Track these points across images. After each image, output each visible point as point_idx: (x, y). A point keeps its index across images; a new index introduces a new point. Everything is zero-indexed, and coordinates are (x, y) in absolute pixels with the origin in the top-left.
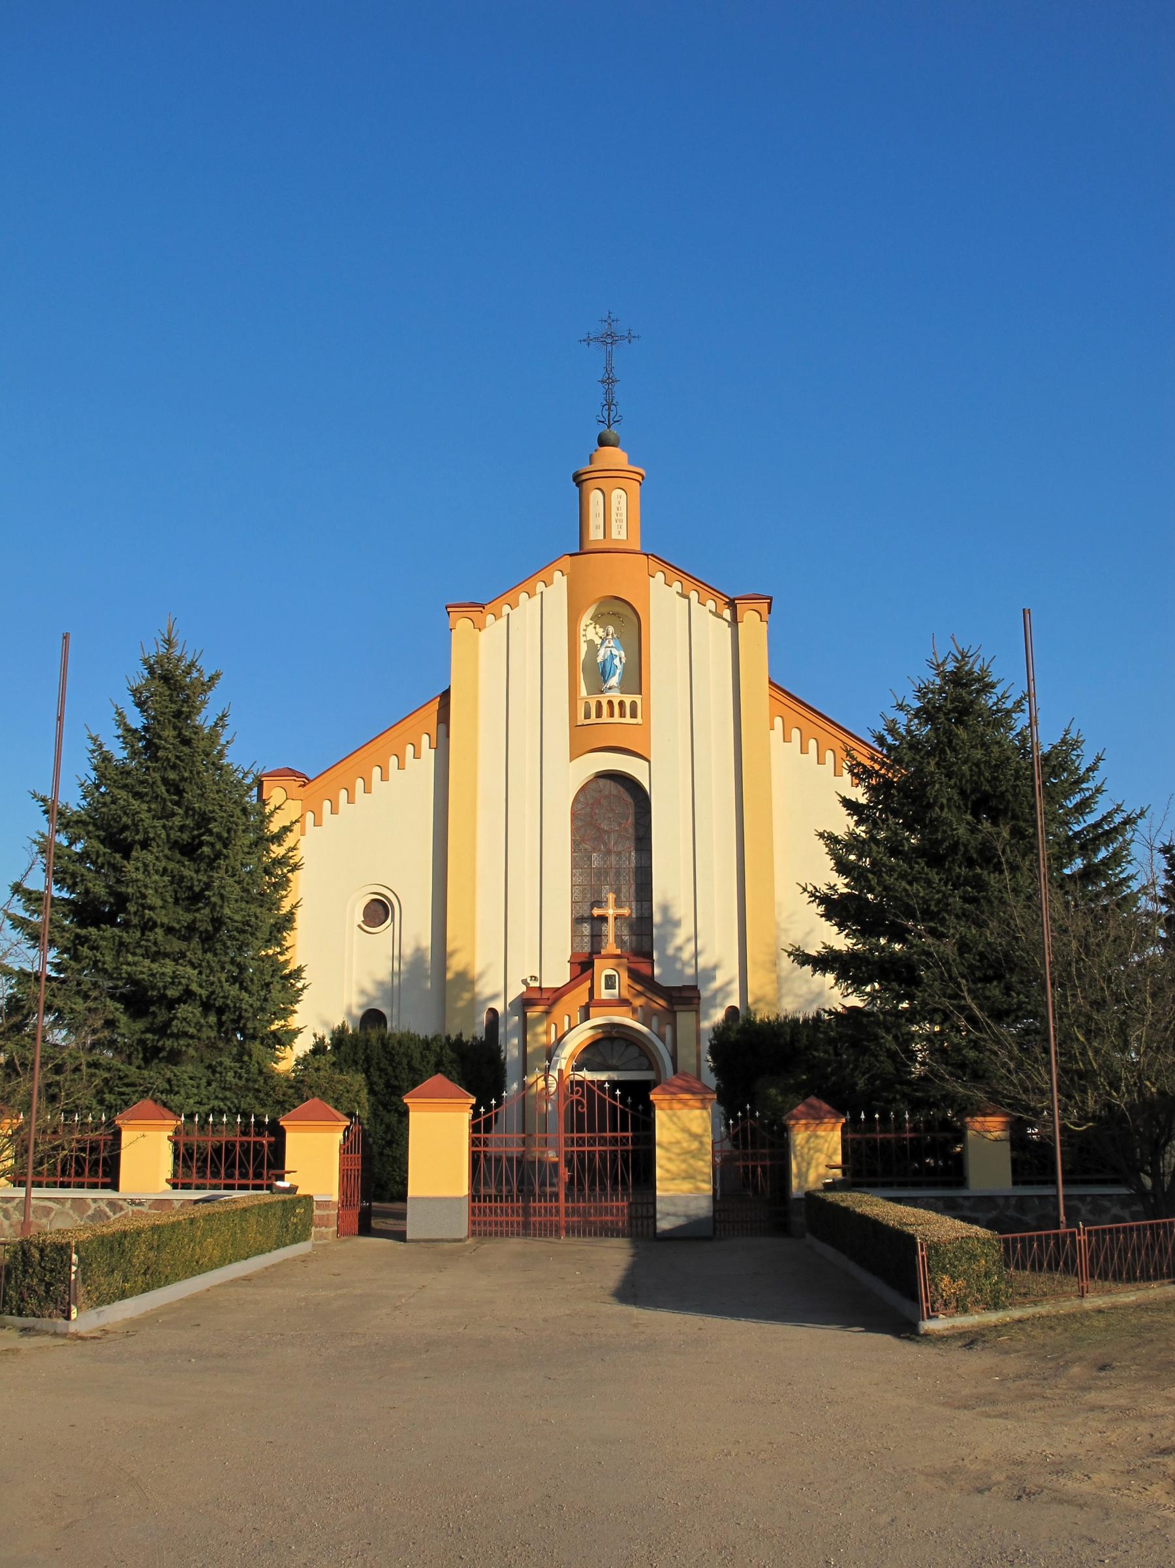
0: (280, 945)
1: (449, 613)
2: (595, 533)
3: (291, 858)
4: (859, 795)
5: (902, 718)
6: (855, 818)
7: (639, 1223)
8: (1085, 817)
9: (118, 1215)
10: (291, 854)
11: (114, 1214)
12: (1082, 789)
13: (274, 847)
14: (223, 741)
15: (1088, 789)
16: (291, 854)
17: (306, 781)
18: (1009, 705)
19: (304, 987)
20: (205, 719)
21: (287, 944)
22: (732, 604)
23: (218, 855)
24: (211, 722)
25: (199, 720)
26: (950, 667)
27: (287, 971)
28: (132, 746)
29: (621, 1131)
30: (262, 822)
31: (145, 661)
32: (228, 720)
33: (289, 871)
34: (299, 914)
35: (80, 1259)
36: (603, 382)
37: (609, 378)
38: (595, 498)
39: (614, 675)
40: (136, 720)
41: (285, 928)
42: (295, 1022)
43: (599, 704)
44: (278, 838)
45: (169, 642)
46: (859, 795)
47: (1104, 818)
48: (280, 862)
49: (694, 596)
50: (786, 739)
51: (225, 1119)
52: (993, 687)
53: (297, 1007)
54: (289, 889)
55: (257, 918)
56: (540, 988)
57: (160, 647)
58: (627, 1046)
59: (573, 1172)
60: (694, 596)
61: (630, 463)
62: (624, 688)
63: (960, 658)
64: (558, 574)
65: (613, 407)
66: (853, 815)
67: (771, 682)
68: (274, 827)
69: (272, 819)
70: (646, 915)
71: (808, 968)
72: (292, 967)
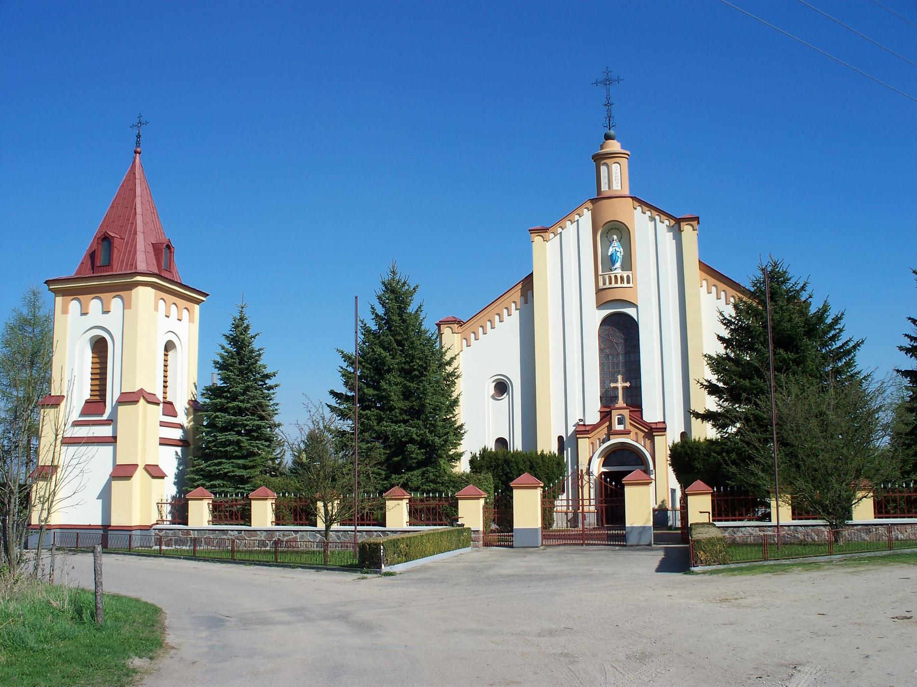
0: (452, 413)
2: (604, 187)
4: (726, 334)
6: (725, 345)
7: (619, 539)
10: (456, 371)
13: (447, 367)
14: (421, 318)
16: (456, 371)
17: (460, 323)
19: (465, 432)
20: (412, 309)
22: (678, 221)
23: (422, 374)
26: (769, 269)
30: (441, 357)
31: (383, 283)
33: (455, 378)
34: (461, 399)
35: (384, 547)
37: (608, 103)
38: (603, 169)
39: (617, 262)
40: (380, 311)
42: (460, 449)
43: (610, 278)
44: (449, 363)
45: (393, 272)
46: (726, 334)
47: (843, 345)
48: (452, 374)
49: (657, 218)
50: (709, 292)
51: (431, 495)
54: (455, 387)
55: (441, 403)
56: (584, 425)
57: (390, 276)
60: (657, 218)
61: (622, 148)
62: (623, 268)
64: (585, 210)
65: (611, 118)
66: (724, 344)
67: (699, 261)
68: (447, 358)
72: (458, 424)
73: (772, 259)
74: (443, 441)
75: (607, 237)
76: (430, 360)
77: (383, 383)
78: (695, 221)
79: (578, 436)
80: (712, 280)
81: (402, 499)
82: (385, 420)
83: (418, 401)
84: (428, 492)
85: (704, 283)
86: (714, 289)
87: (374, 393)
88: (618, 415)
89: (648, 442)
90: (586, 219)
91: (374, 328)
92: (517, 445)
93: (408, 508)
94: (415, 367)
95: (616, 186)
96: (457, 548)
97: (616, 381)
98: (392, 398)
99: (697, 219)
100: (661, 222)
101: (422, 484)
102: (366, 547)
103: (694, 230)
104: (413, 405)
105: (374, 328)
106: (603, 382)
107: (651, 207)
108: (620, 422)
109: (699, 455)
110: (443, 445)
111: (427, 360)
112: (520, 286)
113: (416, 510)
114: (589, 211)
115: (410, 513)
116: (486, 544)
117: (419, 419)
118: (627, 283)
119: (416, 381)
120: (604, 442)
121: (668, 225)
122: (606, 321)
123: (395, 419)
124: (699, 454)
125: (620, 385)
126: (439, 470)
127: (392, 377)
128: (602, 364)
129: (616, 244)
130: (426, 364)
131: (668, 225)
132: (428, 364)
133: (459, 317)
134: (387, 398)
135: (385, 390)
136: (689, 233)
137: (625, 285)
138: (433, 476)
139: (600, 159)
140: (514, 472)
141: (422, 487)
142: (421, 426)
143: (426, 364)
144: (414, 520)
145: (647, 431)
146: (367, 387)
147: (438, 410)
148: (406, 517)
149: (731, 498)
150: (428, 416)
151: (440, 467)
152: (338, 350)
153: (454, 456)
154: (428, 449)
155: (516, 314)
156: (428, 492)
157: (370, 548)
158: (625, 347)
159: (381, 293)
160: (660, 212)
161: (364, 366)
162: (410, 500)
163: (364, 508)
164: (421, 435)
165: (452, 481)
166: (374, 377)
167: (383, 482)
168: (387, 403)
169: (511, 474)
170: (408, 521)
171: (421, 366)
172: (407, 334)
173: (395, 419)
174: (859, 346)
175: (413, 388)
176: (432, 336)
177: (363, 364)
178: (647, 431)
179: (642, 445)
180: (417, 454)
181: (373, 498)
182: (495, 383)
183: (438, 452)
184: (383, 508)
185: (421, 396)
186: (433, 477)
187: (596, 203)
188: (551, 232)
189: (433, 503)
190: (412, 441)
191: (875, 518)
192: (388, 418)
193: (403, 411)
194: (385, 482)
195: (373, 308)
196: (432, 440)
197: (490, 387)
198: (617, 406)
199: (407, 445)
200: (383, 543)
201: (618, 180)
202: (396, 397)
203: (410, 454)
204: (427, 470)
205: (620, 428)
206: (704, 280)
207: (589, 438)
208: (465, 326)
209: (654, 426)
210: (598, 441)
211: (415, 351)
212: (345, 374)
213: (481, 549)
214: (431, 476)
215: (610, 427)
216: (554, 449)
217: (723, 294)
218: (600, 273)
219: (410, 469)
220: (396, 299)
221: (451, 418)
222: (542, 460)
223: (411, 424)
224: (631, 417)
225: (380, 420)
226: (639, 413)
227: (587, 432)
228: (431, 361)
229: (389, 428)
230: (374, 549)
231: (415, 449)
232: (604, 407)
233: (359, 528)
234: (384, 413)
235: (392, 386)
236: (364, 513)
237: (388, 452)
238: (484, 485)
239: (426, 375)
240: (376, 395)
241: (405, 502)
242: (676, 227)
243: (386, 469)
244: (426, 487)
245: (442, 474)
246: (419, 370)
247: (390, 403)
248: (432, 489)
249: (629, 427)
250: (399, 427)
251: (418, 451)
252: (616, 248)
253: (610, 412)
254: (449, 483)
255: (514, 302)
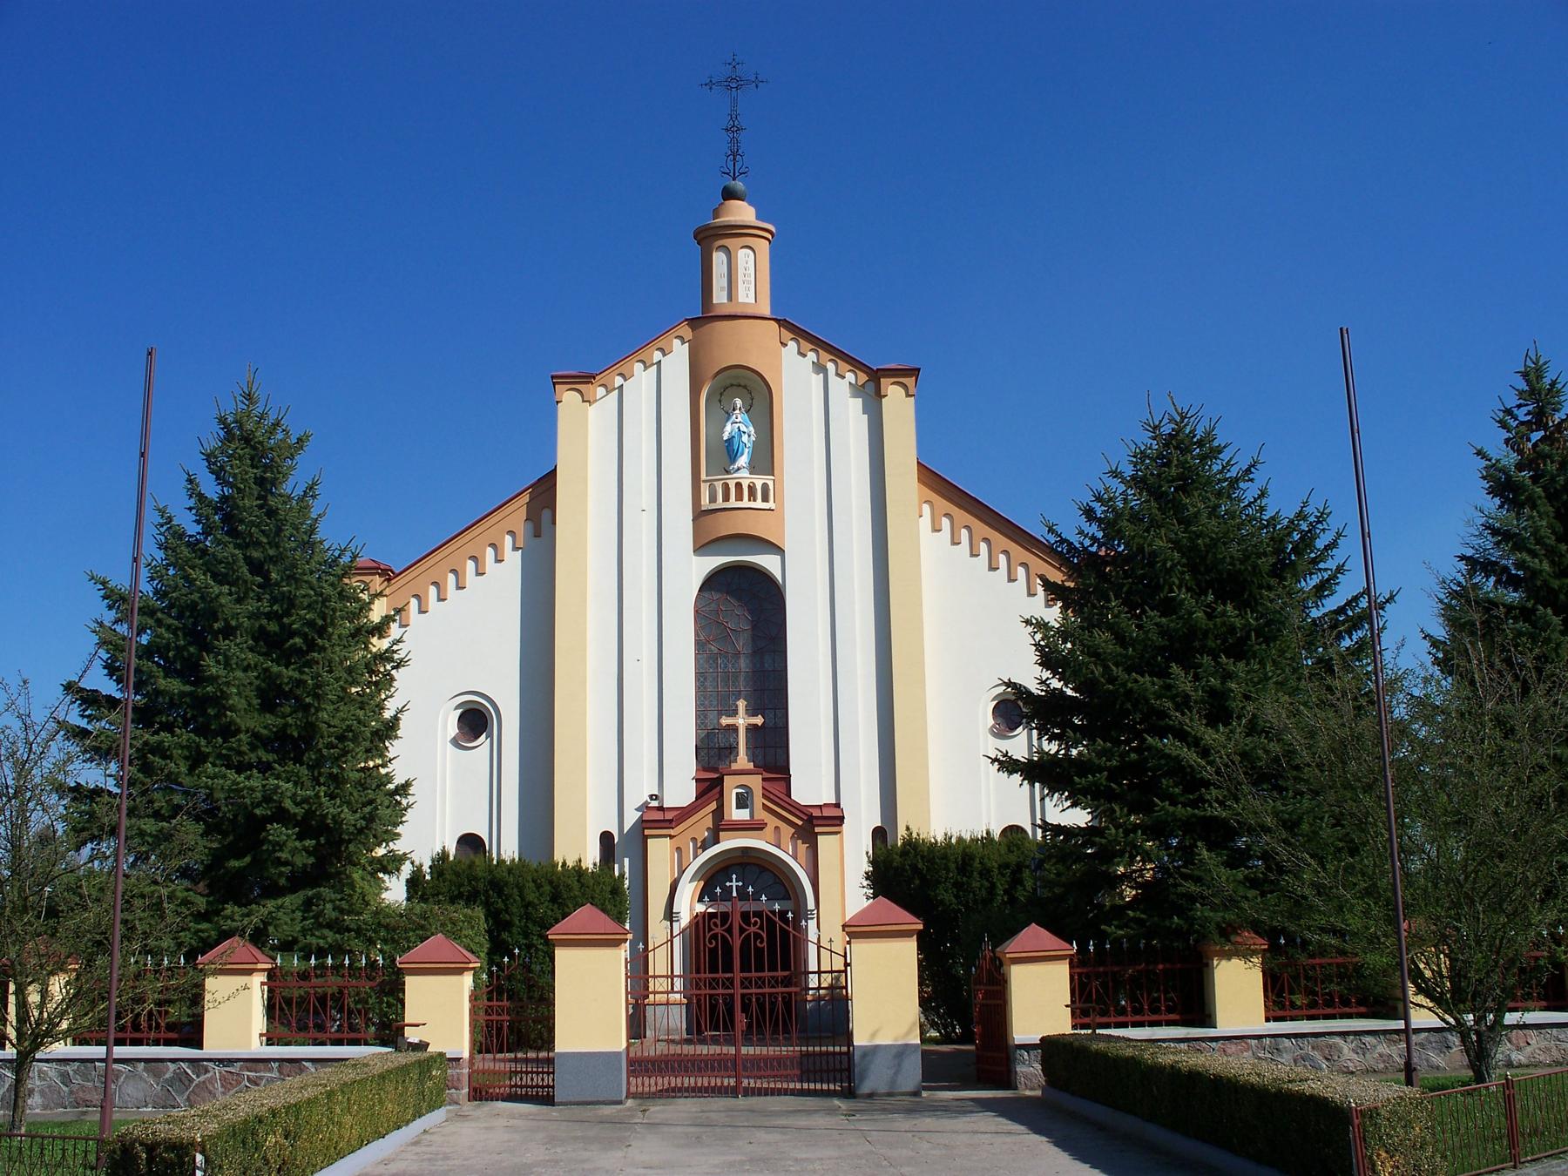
0: (382, 756)
1: (554, 384)
2: (719, 296)
3: (395, 652)
5: (1118, 487)
8: (1323, 601)
9: (202, 1078)
10: (395, 648)
11: (198, 1077)
12: (1320, 570)
13: (374, 640)
15: (1326, 570)
16: (395, 648)
18: (1233, 473)
20: (293, 485)
21: (390, 755)
23: (312, 646)
24: (299, 491)
25: (287, 488)
26: (1167, 429)
27: (391, 787)
28: (208, 519)
29: (769, 971)
31: (222, 421)
32: (318, 489)
33: (393, 668)
35: (207, 1160)
36: (727, 130)
38: (719, 259)
39: (742, 454)
40: (211, 489)
41: (389, 738)
42: (399, 846)
43: (726, 488)
44: (380, 629)
45: (249, 397)
47: (1349, 603)
48: (385, 656)
49: (831, 367)
51: (330, 961)
52: (1220, 452)
53: (399, 829)
55: (359, 722)
56: (661, 808)
58: (761, 873)
59: (751, 1018)
60: (831, 367)
61: (757, 219)
62: (754, 468)
63: (1178, 419)
64: (677, 342)
67: (918, 462)
69: (372, 606)
70: (781, 725)
71: (1017, 777)
72: (399, 780)
73: (1176, 410)
74: (363, 818)
75: (720, 401)
76: (334, 610)
77: (208, 660)
78: (911, 376)
79: (647, 832)
80: (944, 505)
81: (249, 972)
82: (210, 759)
83: (300, 715)
84: (321, 953)
85: (926, 508)
86: (946, 522)
87: (182, 688)
88: (737, 787)
89: (802, 848)
90: (677, 360)
91: (193, 529)
92: (509, 848)
93: (265, 996)
94: (294, 626)
95: (746, 296)
96: (418, 1114)
97: (735, 713)
98: (231, 702)
99: (914, 372)
100: (838, 374)
101: (304, 932)
102: (137, 1157)
103: (908, 395)
104: (286, 725)
105: (193, 529)
106: (701, 715)
107: (819, 344)
108: (742, 802)
109: (947, 873)
110: (361, 831)
111: (326, 607)
112: (526, 498)
113: (289, 1002)
114: (683, 343)
115: (270, 1009)
116: (479, 1094)
117: (298, 760)
118: (763, 501)
119: (295, 663)
120: (704, 847)
121: (854, 382)
122: (712, 583)
123: (235, 759)
124: (948, 870)
125: (742, 721)
126: (350, 895)
127: (238, 648)
128: (701, 677)
129: (740, 416)
130: (325, 620)
131: (854, 382)
132: (329, 621)
133: (385, 561)
134: (219, 701)
135: (213, 679)
136: (898, 403)
137: (759, 504)
138: (334, 910)
139: (710, 236)
140: (515, 910)
141: (303, 941)
142: (305, 779)
143: (325, 620)
144: (282, 1030)
145: (800, 823)
146: (166, 677)
147: (351, 740)
148: (258, 1022)
149: (1179, 966)
150: (322, 756)
151: (353, 887)
152: (93, 578)
153: (385, 863)
154: (322, 840)
155: (513, 560)
156: (321, 953)
157: (150, 1160)
158: (753, 640)
159: (212, 443)
160: (838, 354)
161: (159, 623)
162: (271, 974)
163: (139, 1000)
164: (306, 800)
165: (383, 926)
166: (184, 648)
167: (199, 927)
168: (217, 716)
169: (507, 912)
170: (265, 1032)
171: (311, 624)
172: (277, 546)
173: (235, 759)
174: (1383, 609)
175: (286, 680)
176: (339, 556)
177: (159, 615)
178: (800, 823)
179: (788, 855)
180: (294, 851)
181: (169, 969)
182: (459, 711)
183: (347, 848)
184: (196, 999)
185: (307, 700)
186: (334, 915)
187: (701, 326)
188: (599, 383)
189: (332, 983)
190: (281, 816)
191: (1267, 1020)
192: (220, 756)
193: (258, 740)
194: (205, 926)
195: (190, 481)
196: (334, 816)
197: (449, 724)
198: (734, 767)
199: (269, 827)
200: (202, 1144)
201: (749, 275)
202: (243, 701)
203: (276, 851)
204: (319, 896)
205: (741, 815)
206: (925, 502)
207: (671, 837)
208: (398, 583)
209: (816, 813)
210: (691, 844)
211: (297, 589)
212: (110, 642)
213: (465, 1108)
214: (329, 912)
215: (719, 813)
216: (591, 857)
217: (964, 533)
218: (703, 477)
219: (273, 891)
220: (254, 462)
221: (376, 767)
222: (578, 881)
223: (279, 774)
224: (767, 794)
225: (196, 760)
226: (783, 783)
227: (667, 825)
228: (338, 614)
229: (221, 781)
230: (169, 1165)
231: (288, 836)
232: (705, 769)
233: (120, 1051)
234: (208, 743)
235: (232, 669)
236: (139, 1015)
237: (215, 845)
238: (466, 937)
239: (323, 649)
240: (190, 694)
241: (258, 980)
242: (871, 387)
243: (207, 891)
244: (314, 941)
245: (357, 907)
246: (305, 636)
247: (226, 716)
248: (330, 946)
249: (761, 815)
250: (248, 778)
251: (297, 844)
252: (740, 426)
253: (720, 781)
254: (375, 931)
255: (511, 533)
